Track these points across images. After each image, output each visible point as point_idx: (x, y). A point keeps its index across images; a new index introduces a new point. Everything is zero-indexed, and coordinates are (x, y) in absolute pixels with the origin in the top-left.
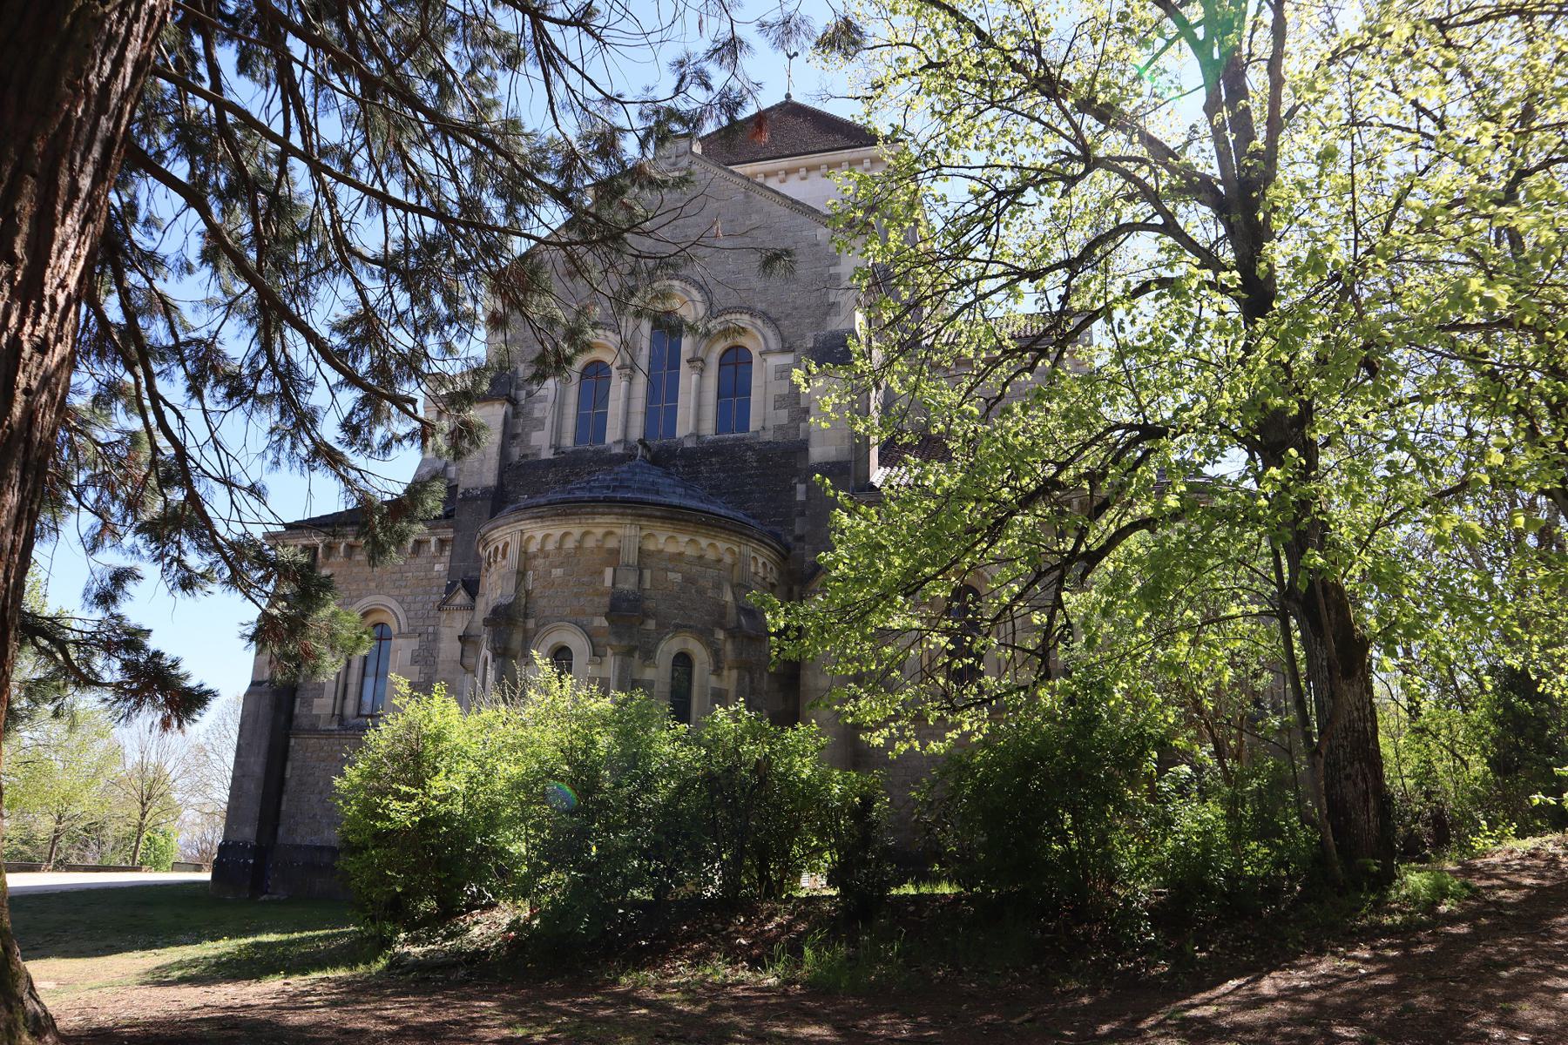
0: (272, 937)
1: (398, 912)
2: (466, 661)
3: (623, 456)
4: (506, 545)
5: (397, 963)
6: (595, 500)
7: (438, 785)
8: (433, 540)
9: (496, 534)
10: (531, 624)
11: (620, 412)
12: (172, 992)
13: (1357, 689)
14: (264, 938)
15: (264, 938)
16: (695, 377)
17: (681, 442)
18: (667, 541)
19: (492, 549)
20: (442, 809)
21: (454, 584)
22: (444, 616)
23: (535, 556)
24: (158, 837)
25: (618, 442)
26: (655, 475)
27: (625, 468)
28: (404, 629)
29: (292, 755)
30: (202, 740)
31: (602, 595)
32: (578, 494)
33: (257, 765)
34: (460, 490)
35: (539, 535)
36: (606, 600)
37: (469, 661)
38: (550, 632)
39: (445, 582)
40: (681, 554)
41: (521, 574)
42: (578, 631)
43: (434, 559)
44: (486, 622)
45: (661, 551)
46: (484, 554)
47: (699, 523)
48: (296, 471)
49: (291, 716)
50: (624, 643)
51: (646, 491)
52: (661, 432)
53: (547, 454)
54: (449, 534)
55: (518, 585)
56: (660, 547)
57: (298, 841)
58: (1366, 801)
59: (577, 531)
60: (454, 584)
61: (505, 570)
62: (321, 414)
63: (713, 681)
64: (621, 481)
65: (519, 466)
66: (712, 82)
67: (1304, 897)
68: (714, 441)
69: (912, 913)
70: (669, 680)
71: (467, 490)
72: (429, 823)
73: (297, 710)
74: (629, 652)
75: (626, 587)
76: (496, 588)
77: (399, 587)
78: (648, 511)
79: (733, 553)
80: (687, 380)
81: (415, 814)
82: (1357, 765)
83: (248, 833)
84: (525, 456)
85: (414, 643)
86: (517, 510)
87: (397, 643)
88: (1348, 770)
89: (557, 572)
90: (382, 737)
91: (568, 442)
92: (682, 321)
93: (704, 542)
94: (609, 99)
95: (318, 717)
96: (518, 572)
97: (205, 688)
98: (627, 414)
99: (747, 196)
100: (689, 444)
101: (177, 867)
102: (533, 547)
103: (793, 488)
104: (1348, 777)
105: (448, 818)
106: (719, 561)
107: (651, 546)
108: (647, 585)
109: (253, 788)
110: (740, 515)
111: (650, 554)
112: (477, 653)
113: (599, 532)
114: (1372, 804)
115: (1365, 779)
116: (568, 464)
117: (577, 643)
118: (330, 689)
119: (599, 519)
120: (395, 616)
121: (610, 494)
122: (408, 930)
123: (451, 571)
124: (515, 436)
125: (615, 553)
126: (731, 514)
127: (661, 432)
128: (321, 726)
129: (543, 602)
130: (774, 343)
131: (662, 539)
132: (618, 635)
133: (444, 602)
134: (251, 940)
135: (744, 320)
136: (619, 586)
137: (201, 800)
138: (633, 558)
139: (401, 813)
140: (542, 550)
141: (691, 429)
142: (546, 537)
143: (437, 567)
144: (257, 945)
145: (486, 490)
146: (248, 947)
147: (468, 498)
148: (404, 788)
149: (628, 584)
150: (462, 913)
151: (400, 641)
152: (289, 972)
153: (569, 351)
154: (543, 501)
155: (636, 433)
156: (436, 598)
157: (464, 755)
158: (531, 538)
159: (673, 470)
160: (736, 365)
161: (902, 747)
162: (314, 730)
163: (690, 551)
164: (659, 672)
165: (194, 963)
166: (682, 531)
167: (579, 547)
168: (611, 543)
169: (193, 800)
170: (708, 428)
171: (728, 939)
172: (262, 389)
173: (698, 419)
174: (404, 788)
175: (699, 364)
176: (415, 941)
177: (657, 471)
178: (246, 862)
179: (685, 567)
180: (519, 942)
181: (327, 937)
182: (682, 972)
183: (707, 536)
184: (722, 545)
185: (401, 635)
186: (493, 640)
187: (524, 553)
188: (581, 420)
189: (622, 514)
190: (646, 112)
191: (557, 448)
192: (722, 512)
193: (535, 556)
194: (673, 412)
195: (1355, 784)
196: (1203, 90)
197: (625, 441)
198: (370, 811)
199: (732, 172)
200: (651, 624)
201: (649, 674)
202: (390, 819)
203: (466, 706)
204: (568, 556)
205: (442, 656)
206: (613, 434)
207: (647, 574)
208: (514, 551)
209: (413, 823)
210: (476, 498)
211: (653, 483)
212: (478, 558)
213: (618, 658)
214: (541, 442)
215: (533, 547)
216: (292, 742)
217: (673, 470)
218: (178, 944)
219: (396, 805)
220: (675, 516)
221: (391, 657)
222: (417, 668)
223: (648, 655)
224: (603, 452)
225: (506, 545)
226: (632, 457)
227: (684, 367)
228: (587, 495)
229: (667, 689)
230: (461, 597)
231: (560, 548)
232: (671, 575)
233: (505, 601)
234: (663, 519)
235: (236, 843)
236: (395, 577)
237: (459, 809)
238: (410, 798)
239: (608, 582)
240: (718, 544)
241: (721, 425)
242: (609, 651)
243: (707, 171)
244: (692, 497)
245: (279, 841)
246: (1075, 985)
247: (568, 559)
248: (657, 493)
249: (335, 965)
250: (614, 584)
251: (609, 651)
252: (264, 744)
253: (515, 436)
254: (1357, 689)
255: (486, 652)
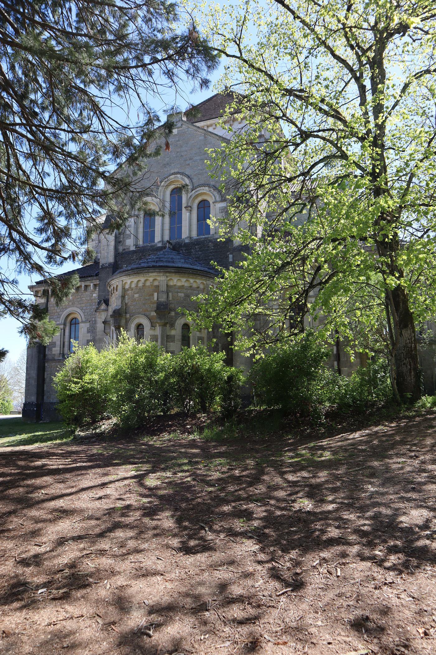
0: (40, 433)
1: (77, 421)
2: (106, 331)
3: (162, 247)
4: (117, 286)
5: (75, 437)
6: (149, 267)
7: (87, 377)
8: (92, 285)
9: (113, 282)
10: (128, 316)
11: (160, 230)
12: (4, 448)
13: (409, 332)
14: (37, 434)
15: (37, 434)
16: (188, 214)
17: (184, 240)
18: (178, 281)
19: (112, 288)
20: (89, 386)
21: (100, 301)
22: (98, 314)
23: (128, 290)
24: (5, 402)
25: (160, 242)
26: (174, 255)
27: (162, 252)
28: (84, 320)
29: (46, 369)
30: (16, 365)
31: (154, 303)
32: (142, 265)
33: (34, 374)
34: (101, 265)
35: (129, 282)
36: (155, 305)
37: (107, 331)
38: (138, 317)
39: (97, 301)
40: (183, 286)
41: (123, 297)
42: (146, 318)
43: (92, 292)
44: (111, 316)
45: (175, 285)
46: (110, 290)
47: (189, 273)
48: (27, 274)
49: (45, 355)
50: (163, 321)
51: (169, 262)
52: (176, 236)
53: (133, 248)
54: (97, 282)
55: (122, 302)
56: (175, 283)
57: (51, 401)
58: (410, 372)
59: (143, 280)
60: (100, 301)
61: (117, 296)
62: (32, 255)
63: (152, 332)
64: (160, 258)
65: (122, 254)
66: (160, 119)
67: (383, 407)
68: (197, 239)
69: (246, 416)
70: (181, 334)
71: (103, 264)
72: (85, 391)
73: (47, 353)
74: (165, 325)
75: (162, 300)
76: (115, 303)
77: (80, 304)
78: (169, 270)
79: (203, 284)
80: (185, 215)
81: (80, 388)
82: (407, 359)
83: (33, 399)
84: (124, 250)
85: (88, 325)
86: (120, 272)
87: (81, 325)
88: (404, 362)
89: (136, 296)
90: (70, 362)
91: (141, 243)
92: (154, 211)
93: (192, 281)
94: (125, 128)
95: (54, 355)
96: (122, 296)
97: (5, 350)
98: (163, 230)
99: (205, 137)
100: (187, 241)
101: (11, 413)
102: (127, 287)
103: (228, 257)
104: (404, 364)
105: (92, 389)
106: (198, 287)
107: (171, 283)
108: (171, 299)
109: (34, 382)
110: (206, 269)
111: (171, 286)
112: (110, 329)
113: (151, 279)
114: (413, 373)
115: (410, 365)
116: (141, 252)
117: (146, 322)
118: (58, 343)
119: (151, 274)
120: (80, 315)
121: (155, 264)
122: (81, 428)
123: (99, 296)
124: (120, 242)
125: (157, 287)
126: (202, 269)
127: (176, 236)
128: (56, 358)
129: (132, 307)
130: (218, 198)
131: (175, 281)
132: (160, 318)
133: (97, 309)
134: (32, 434)
135: (206, 189)
136: (160, 300)
137: (18, 388)
138: (164, 288)
139: (75, 388)
140: (130, 287)
141: (187, 235)
142: (131, 282)
143: (94, 295)
144: (34, 436)
145: (110, 264)
146: (31, 436)
147: (104, 267)
148: (75, 380)
149: (163, 299)
150: (99, 421)
151: (82, 324)
152: (42, 442)
153: (121, 222)
154: (129, 268)
155: (167, 238)
156: (95, 307)
157: (97, 367)
158: (126, 283)
159: (181, 252)
160: (204, 208)
161: (258, 357)
162: (53, 360)
163: (186, 284)
164: (176, 332)
165: (13, 441)
166: (183, 277)
167: (144, 285)
168: (156, 283)
169: (15, 388)
170: (194, 234)
171: (184, 426)
172: (11, 247)
173: (190, 231)
174: (75, 380)
175: (189, 208)
176: (82, 431)
177: (174, 253)
178: (33, 409)
179: (185, 291)
180: (115, 429)
181: (57, 432)
182: (166, 436)
183: (193, 278)
184: (199, 281)
185: (82, 322)
186: (114, 323)
187: (124, 288)
188: (145, 233)
189: (160, 272)
190: (139, 131)
191: (136, 246)
192: (199, 268)
193: (128, 290)
194: (180, 228)
195: (407, 366)
196: (359, 98)
197: (162, 241)
198: (65, 388)
199: (196, 126)
200: (173, 314)
201: (173, 332)
202: (72, 391)
203: (99, 350)
204: (140, 289)
205: (98, 329)
206: (157, 239)
207: (170, 294)
208: (120, 288)
209: (79, 392)
210: (106, 267)
211: (172, 258)
212: (108, 291)
213: (161, 327)
214: (130, 244)
215: (127, 287)
216: (46, 364)
217: (181, 252)
218: (9, 437)
219: (73, 385)
220: (180, 271)
221: (80, 330)
222: (89, 334)
223: (172, 325)
224: (154, 246)
225: (117, 286)
226: (165, 247)
227: (184, 210)
228: (146, 265)
229: (180, 338)
230: (103, 306)
231: (137, 286)
232: (180, 294)
233: (118, 308)
234: (175, 272)
235: (29, 403)
236: (78, 300)
237: (95, 385)
238: (76, 383)
239: (156, 299)
240: (198, 281)
241: (199, 234)
242: (158, 325)
243: (188, 128)
244: (187, 263)
245: (45, 401)
246: (290, 437)
247: (140, 290)
248: (173, 262)
249: (56, 439)
250: (158, 299)
251: (158, 325)
252: (36, 366)
253: (120, 242)
254: (409, 332)
255: (113, 328)
